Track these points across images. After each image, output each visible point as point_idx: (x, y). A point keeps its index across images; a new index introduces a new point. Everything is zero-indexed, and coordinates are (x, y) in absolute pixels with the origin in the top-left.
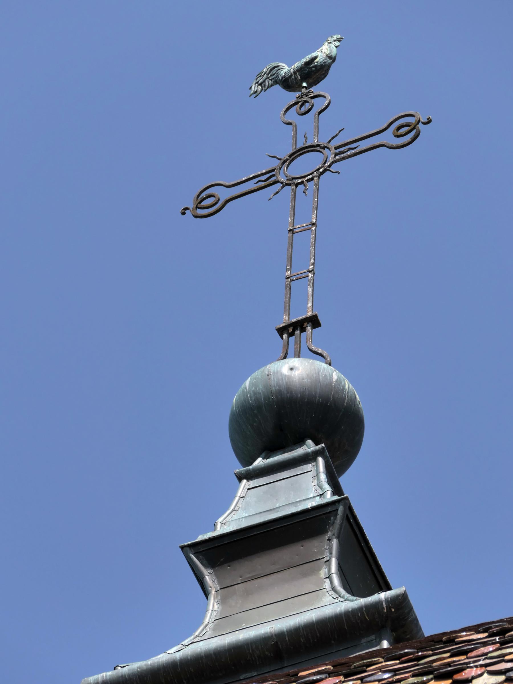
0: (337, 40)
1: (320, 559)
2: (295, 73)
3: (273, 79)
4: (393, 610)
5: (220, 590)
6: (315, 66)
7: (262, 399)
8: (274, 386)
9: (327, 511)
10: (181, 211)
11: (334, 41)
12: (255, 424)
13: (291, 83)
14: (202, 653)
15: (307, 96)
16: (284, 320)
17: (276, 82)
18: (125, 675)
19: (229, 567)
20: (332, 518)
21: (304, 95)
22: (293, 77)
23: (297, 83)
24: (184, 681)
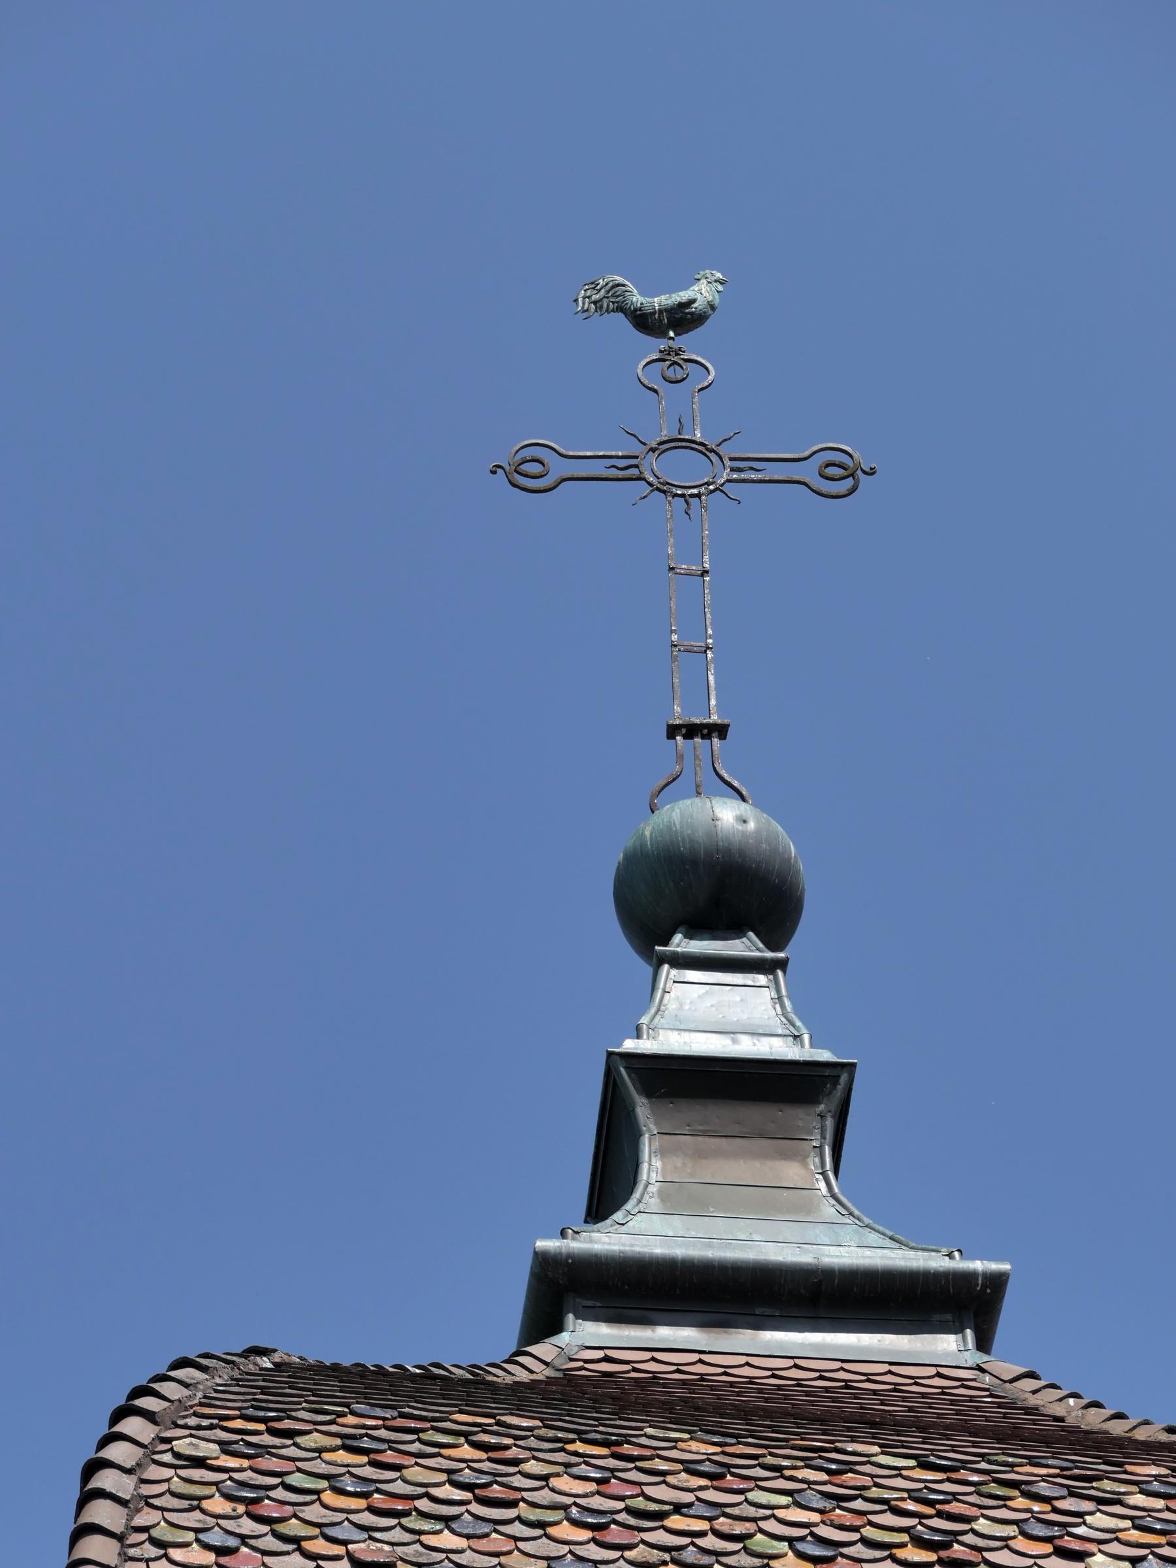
0: (719, 281)
1: (807, 1140)
2: (661, 311)
3: (618, 302)
4: (988, 1291)
5: (657, 1135)
6: (692, 314)
7: (702, 852)
8: (722, 840)
9: (824, 1074)
10: (491, 466)
11: (716, 281)
12: (682, 883)
13: (650, 324)
14: (715, 1261)
15: (677, 354)
16: (679, 714)
17: (621, 309)
18: (601, 1257)
19: (672, 1103)
20: (828, 1086)
21: (672, 351)
22: (657, 316)
23: (660, 327)
24: (678, 1290)
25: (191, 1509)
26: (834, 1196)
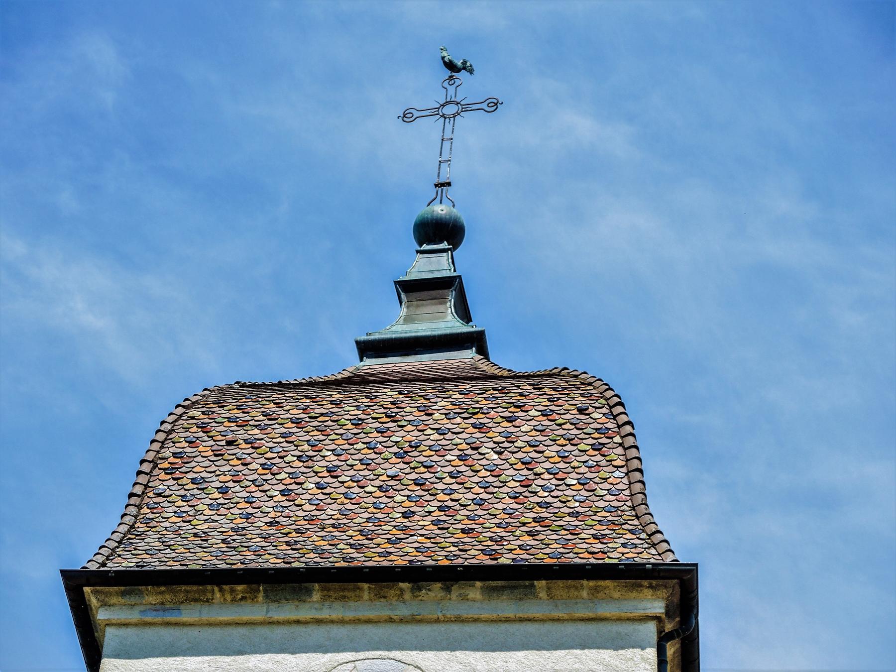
25: (186, 431)
26: (452, 313)
